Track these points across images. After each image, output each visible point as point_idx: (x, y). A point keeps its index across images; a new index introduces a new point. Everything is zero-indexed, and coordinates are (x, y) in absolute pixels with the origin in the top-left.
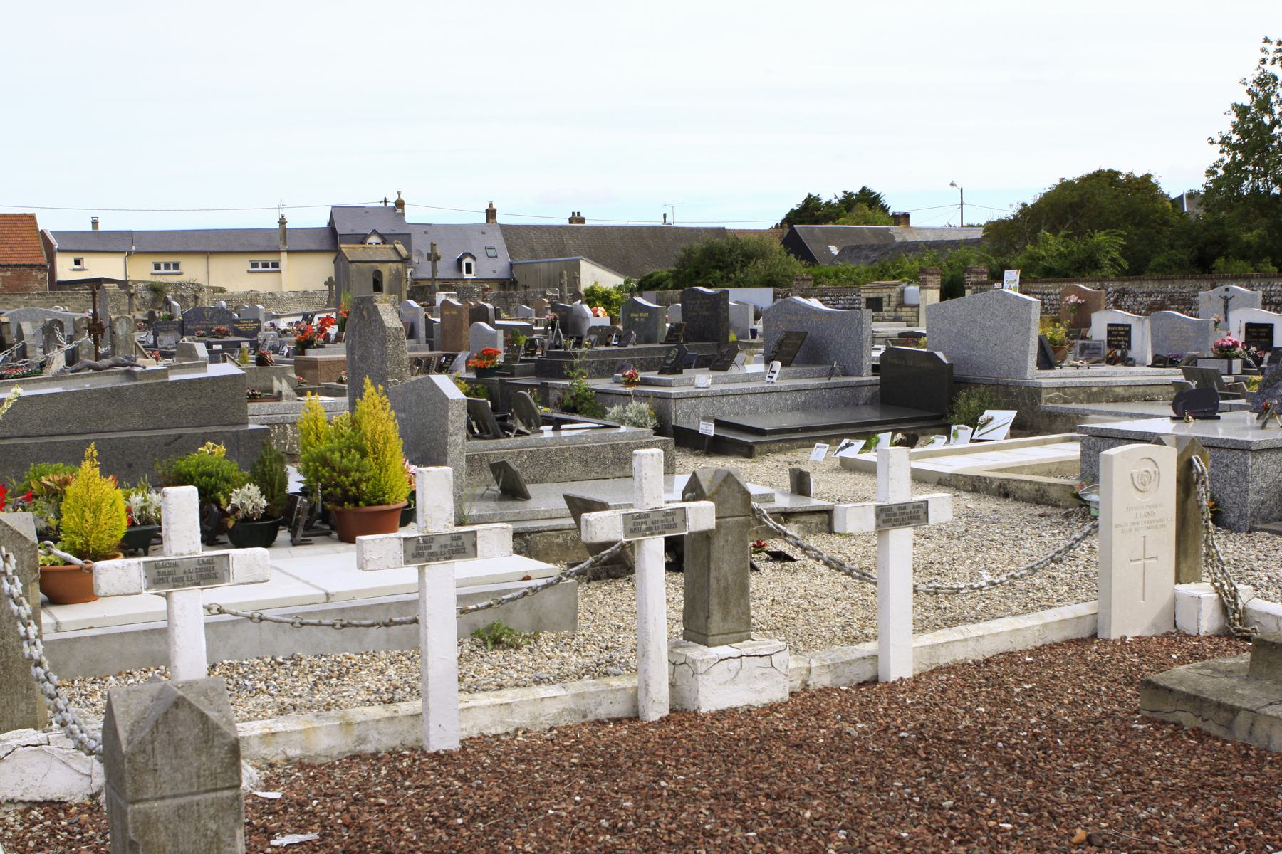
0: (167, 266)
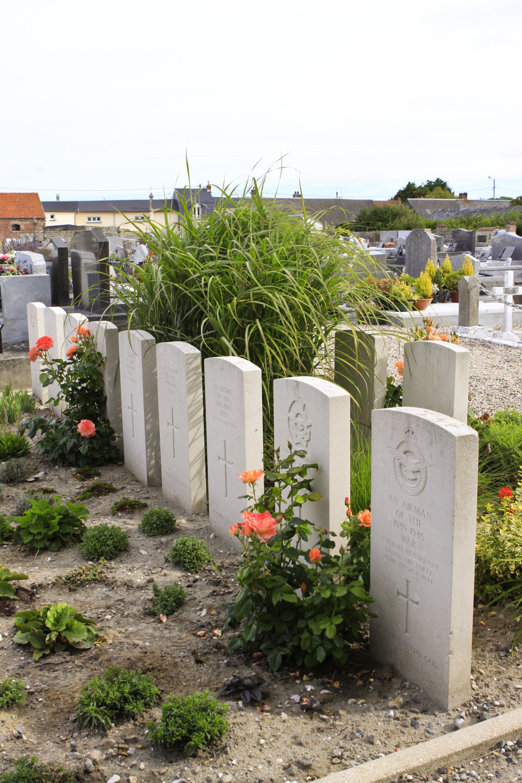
0: (94, 219)
